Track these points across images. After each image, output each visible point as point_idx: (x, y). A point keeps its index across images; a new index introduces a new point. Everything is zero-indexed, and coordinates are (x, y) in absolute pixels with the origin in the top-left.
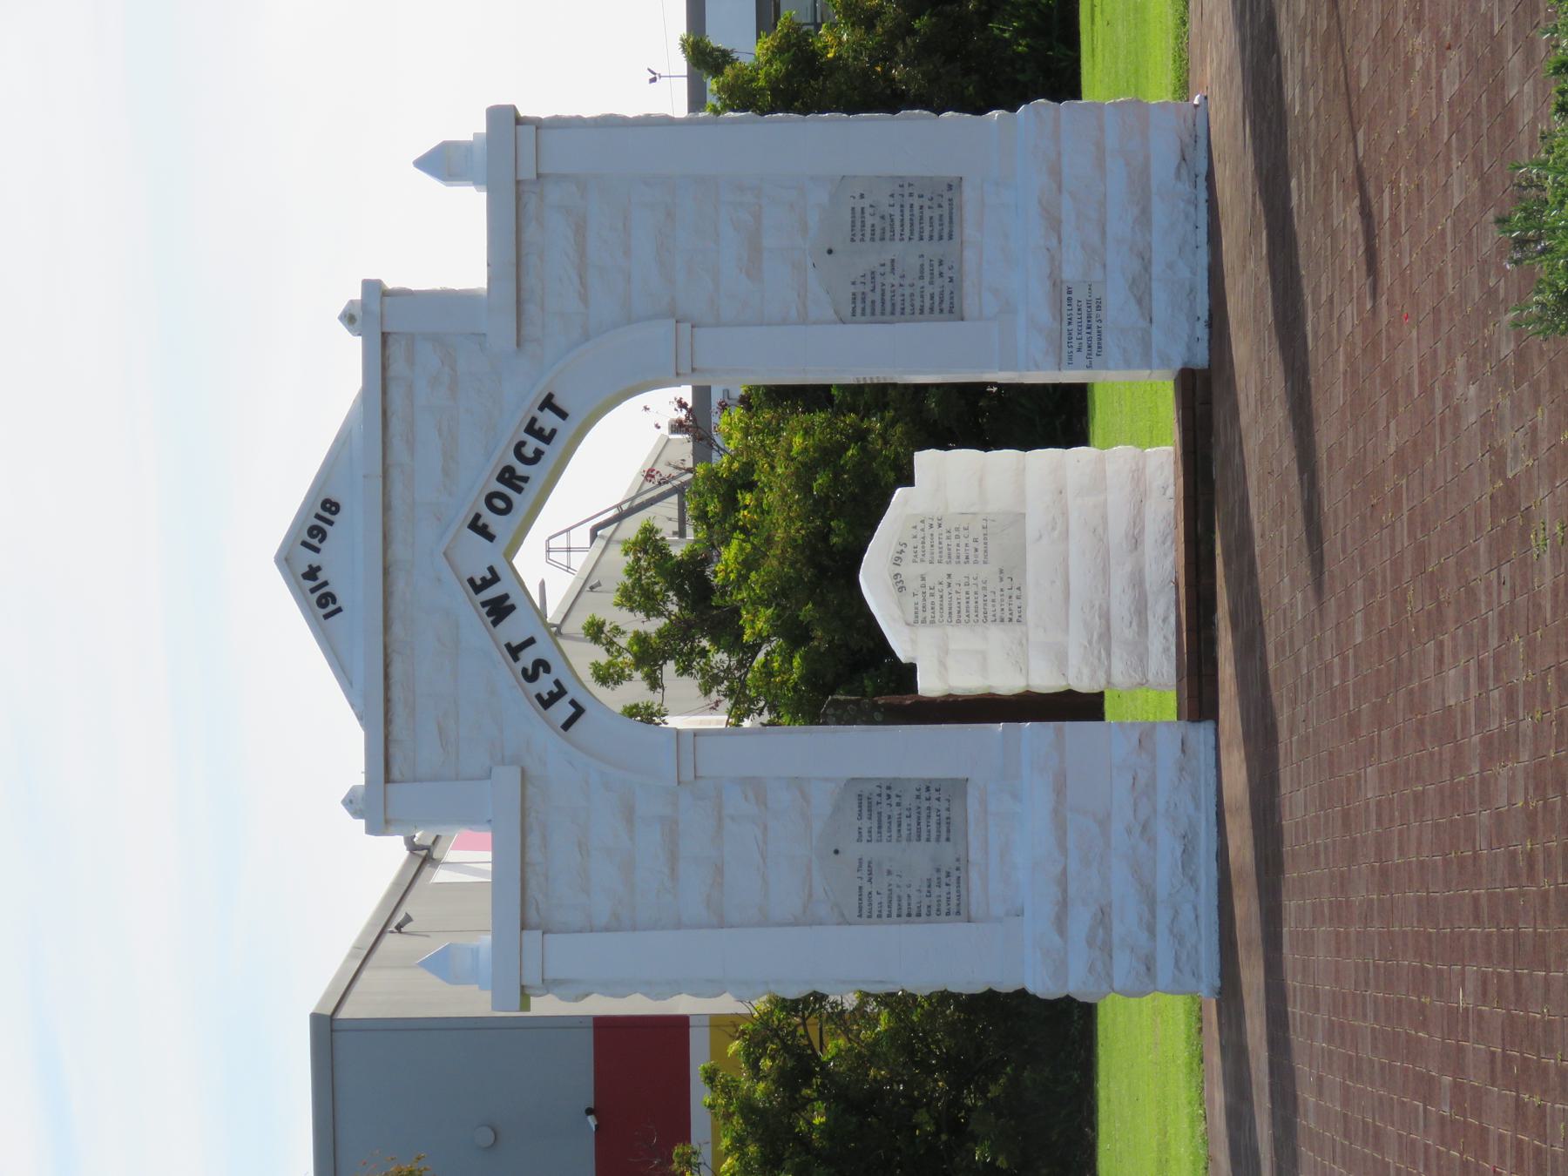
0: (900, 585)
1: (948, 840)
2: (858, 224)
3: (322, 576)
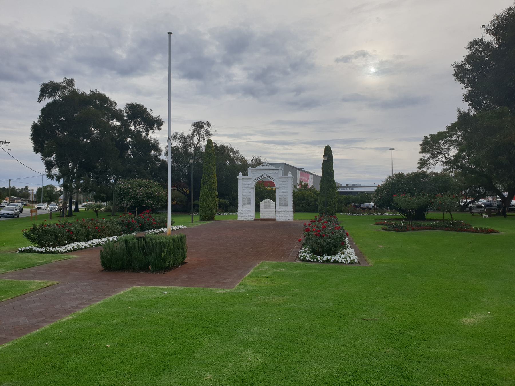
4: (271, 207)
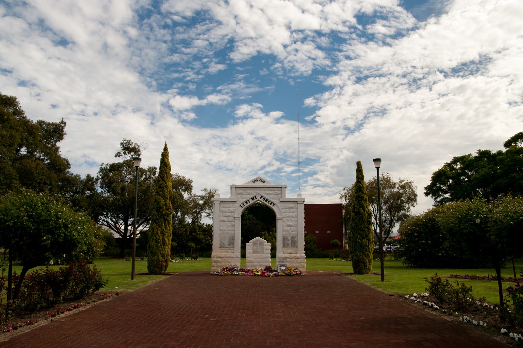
4: (265, 251)
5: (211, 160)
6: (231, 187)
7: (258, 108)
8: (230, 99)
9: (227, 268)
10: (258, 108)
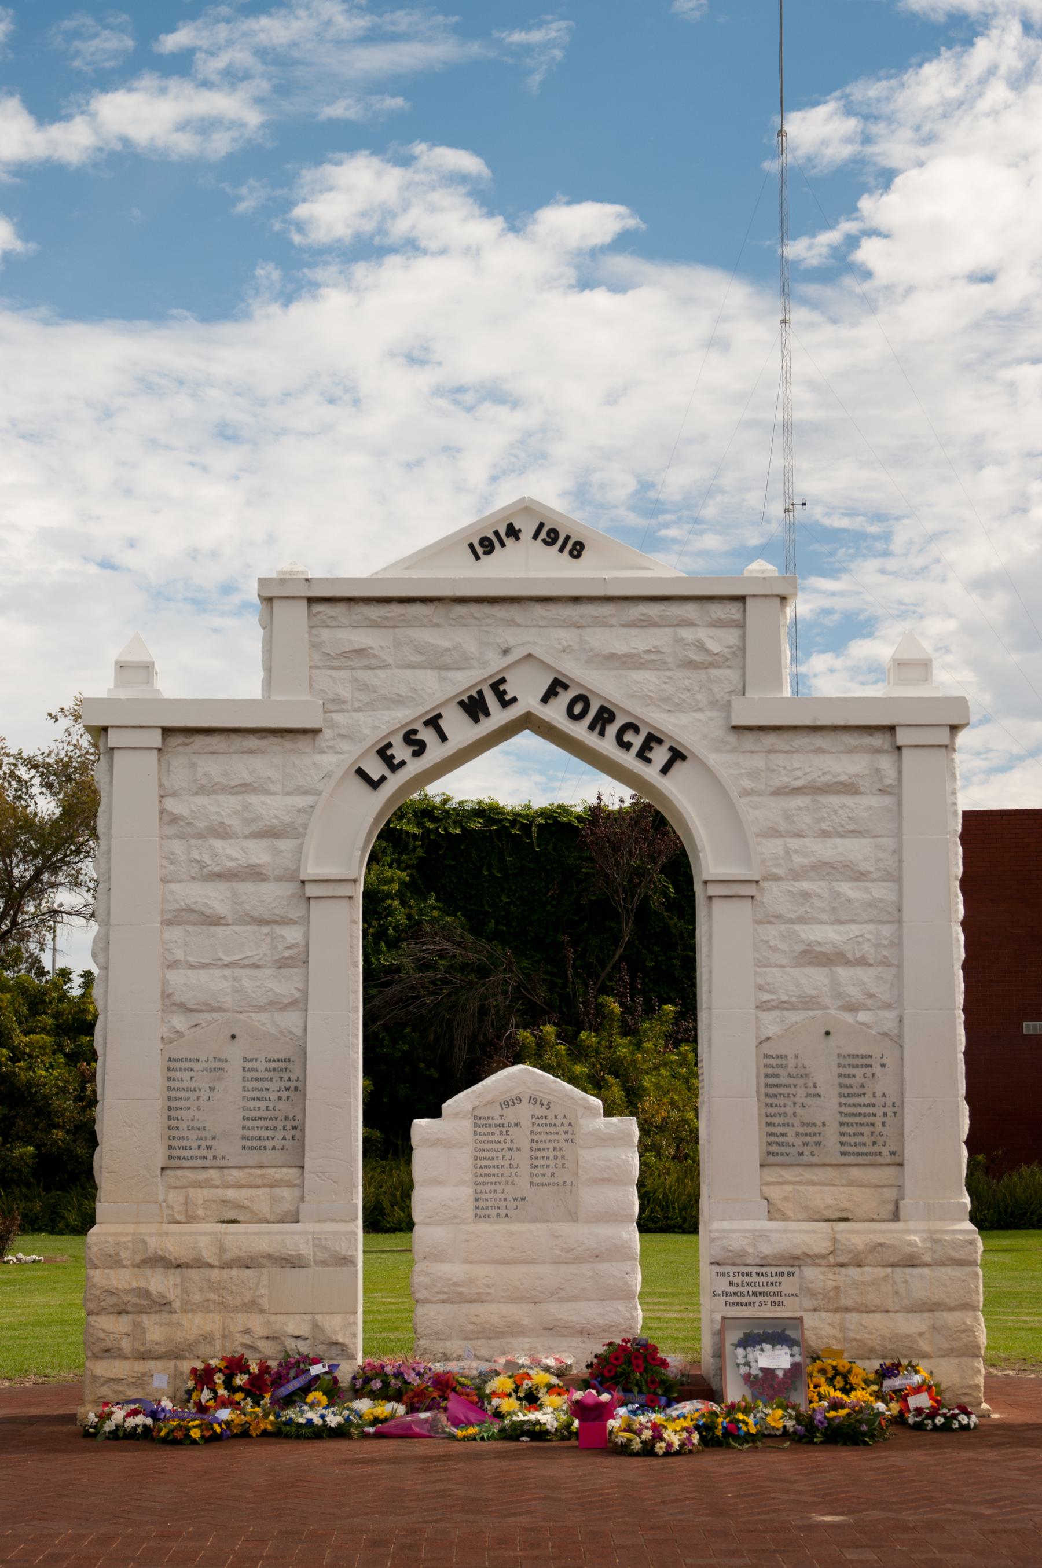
0: (511, 1103)
1: (244, 1148)
2: (855, 1062)
3: (509, 542)
4: (591, 1198)
5: (132, 544)
6: (268, 600)
7: (457, 179)
8: (253, 118)
9: (235, 1365)
10: (457, 179)
